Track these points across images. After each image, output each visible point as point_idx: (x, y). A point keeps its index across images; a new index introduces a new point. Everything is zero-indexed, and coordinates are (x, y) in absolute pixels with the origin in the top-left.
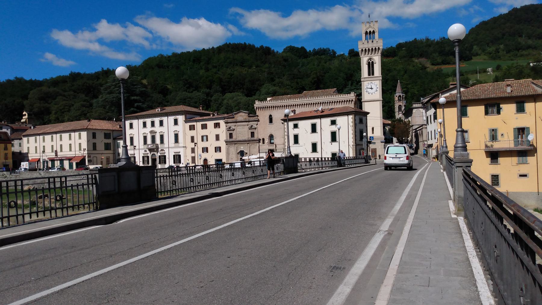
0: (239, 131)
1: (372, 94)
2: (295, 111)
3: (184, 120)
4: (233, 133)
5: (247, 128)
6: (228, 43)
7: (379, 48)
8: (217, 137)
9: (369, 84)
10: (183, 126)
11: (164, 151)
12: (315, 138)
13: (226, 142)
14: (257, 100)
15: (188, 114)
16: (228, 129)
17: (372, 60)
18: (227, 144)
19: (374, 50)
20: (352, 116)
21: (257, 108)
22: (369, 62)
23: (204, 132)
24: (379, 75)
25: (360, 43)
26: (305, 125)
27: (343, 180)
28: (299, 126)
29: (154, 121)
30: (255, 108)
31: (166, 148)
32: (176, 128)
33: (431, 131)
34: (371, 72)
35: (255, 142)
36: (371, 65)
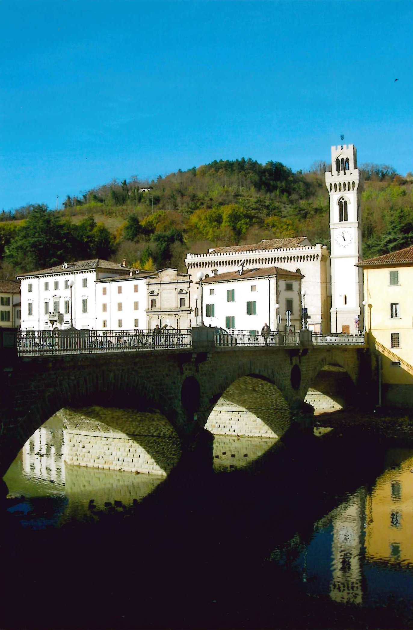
2: (216, 270)
5: (174, 293)
8: (136, 306)
15: (101, 272)
19: (347, 186)
23: (120, 298)
25: (328, 174)
28: (257, 288)
30: (187, 264)
34: (343, 216)
36: (343, 206)
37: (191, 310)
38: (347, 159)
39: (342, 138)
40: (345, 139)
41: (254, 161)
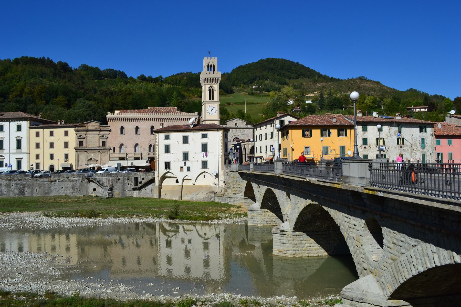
0: (90, 140)
1: (212, 115)
3: (29, 126)
4: (83, 141)
5: (97, 137)
6: (42, 58)
7: (218, 79)
8: (66, 145)
9: (209, 106)
10: (27, 132)
11: (4, 156)
12: (186, 148)
13: (75, 149)
14: (196, 112)
16: (78, 138)
17: (212, 88)
18: (76, 152)
20: (221, 132)
21: (109, 119)
22: (210, 89)
24: (218, 100)
26: (177, 137)
27: (263, 174)
29: (3, 126)
30: (107, 119)
31: (6, 154)
32: (19, 134)
33: (261, 147)
34: (211, 96)
35: (96, 150)
37: (110, 149)
38: (214, 65)
39: (209, 53)
40: (211, 54)
41: (51, 59)
